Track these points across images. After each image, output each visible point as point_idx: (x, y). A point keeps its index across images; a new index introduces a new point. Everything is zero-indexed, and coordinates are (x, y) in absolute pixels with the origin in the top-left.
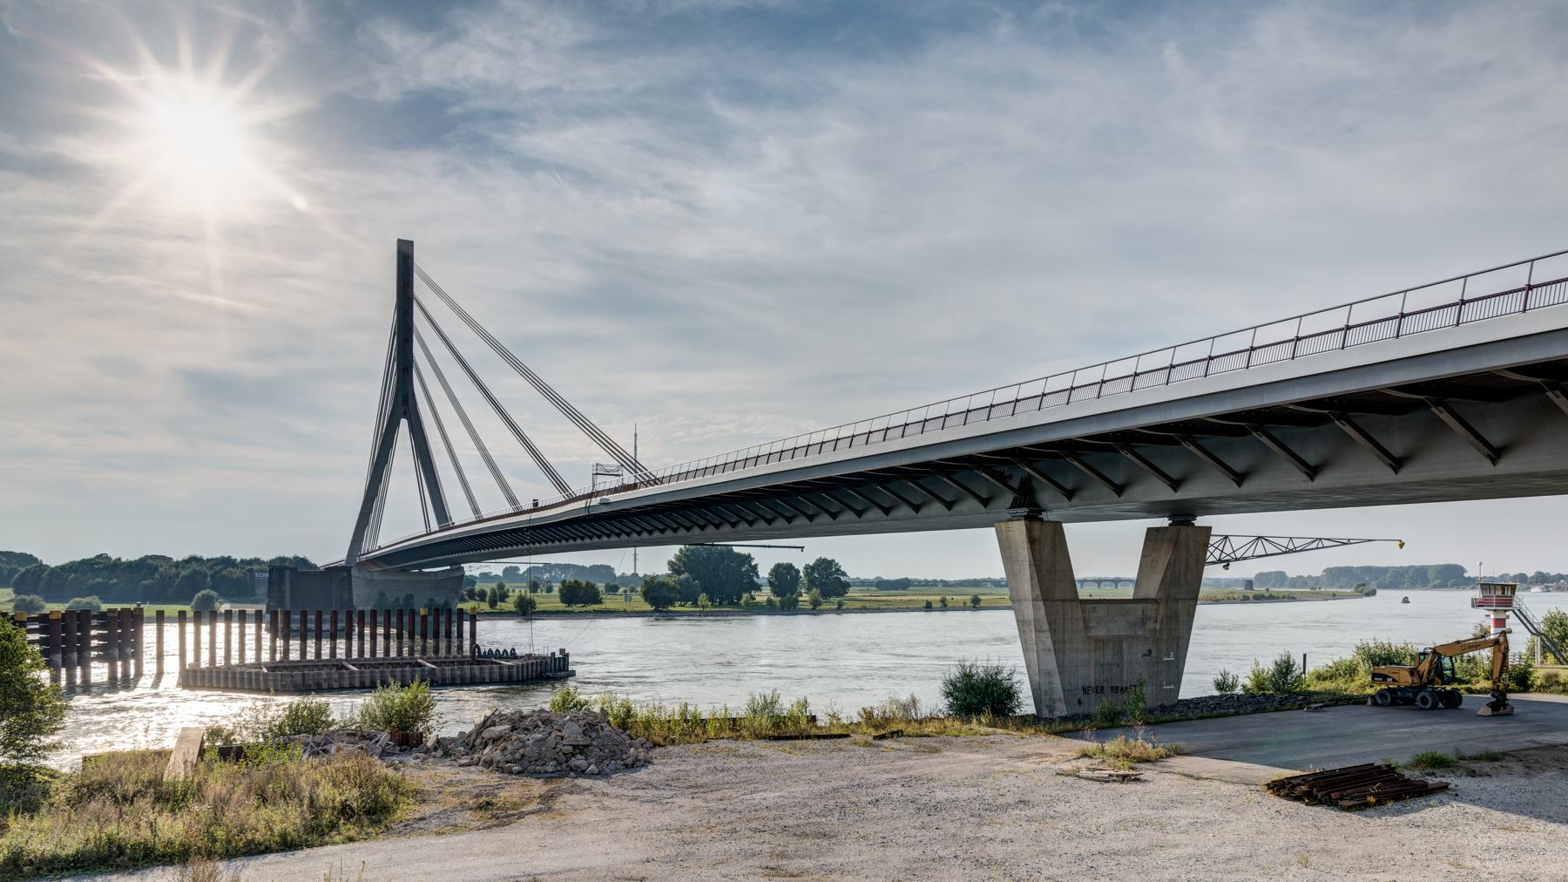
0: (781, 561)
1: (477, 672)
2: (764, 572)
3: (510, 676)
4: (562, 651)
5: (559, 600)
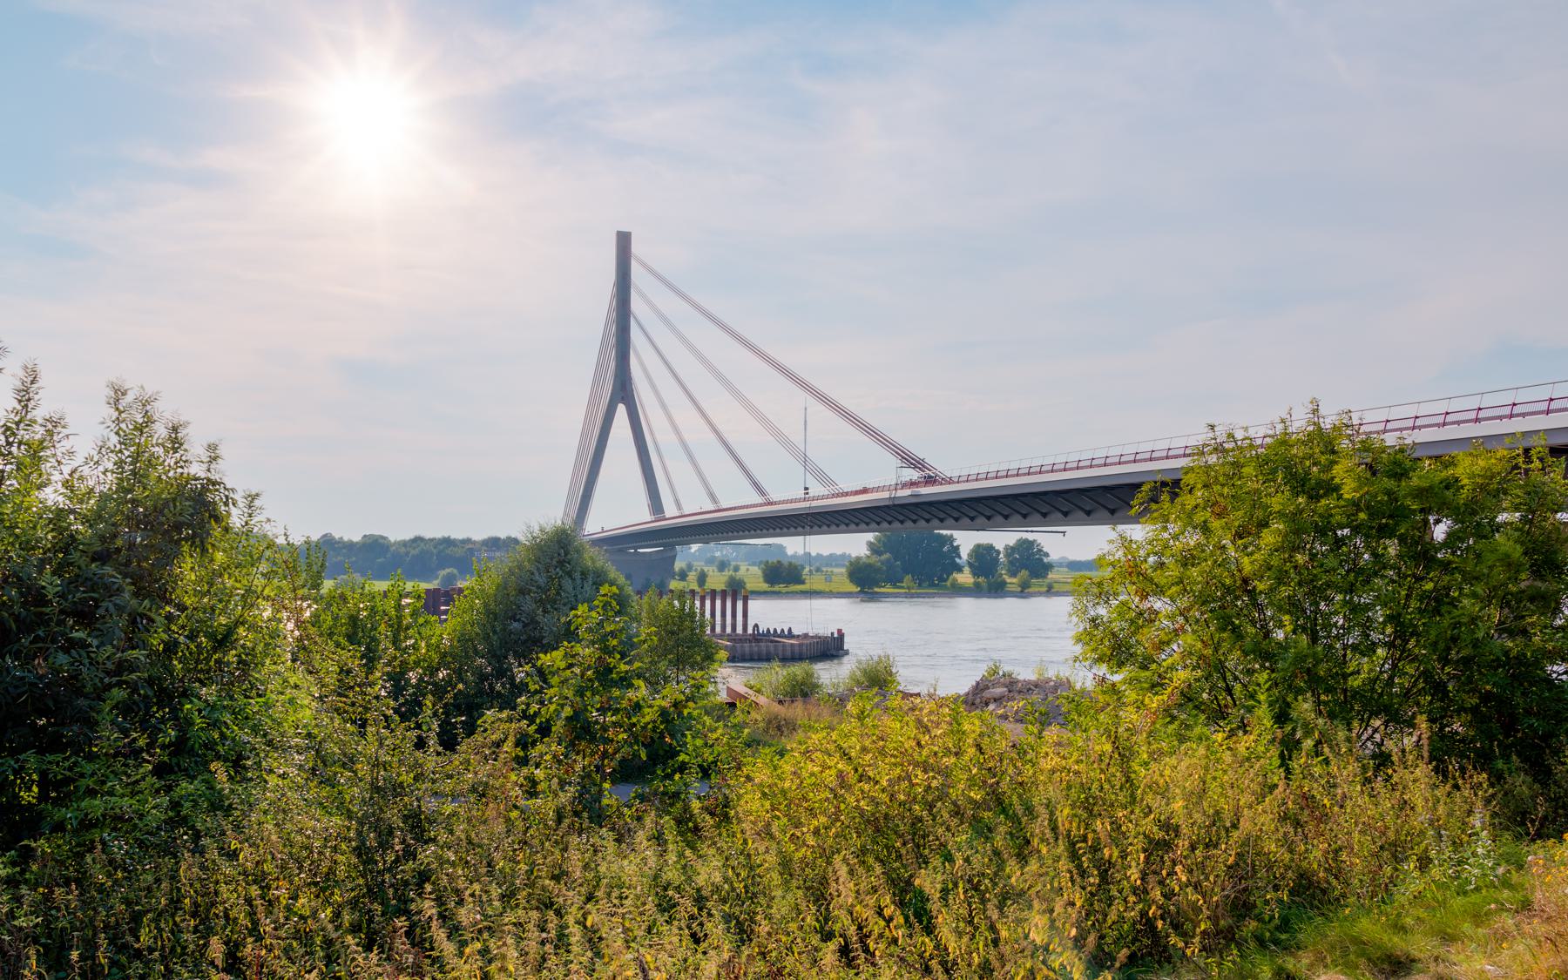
0: (981, 542)
1: (772, 649)
2: (965, 553)
3: (801, 654)
4: (840, 631)
5: (761, 579)
